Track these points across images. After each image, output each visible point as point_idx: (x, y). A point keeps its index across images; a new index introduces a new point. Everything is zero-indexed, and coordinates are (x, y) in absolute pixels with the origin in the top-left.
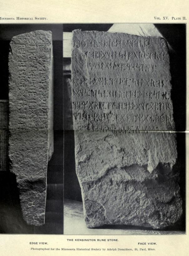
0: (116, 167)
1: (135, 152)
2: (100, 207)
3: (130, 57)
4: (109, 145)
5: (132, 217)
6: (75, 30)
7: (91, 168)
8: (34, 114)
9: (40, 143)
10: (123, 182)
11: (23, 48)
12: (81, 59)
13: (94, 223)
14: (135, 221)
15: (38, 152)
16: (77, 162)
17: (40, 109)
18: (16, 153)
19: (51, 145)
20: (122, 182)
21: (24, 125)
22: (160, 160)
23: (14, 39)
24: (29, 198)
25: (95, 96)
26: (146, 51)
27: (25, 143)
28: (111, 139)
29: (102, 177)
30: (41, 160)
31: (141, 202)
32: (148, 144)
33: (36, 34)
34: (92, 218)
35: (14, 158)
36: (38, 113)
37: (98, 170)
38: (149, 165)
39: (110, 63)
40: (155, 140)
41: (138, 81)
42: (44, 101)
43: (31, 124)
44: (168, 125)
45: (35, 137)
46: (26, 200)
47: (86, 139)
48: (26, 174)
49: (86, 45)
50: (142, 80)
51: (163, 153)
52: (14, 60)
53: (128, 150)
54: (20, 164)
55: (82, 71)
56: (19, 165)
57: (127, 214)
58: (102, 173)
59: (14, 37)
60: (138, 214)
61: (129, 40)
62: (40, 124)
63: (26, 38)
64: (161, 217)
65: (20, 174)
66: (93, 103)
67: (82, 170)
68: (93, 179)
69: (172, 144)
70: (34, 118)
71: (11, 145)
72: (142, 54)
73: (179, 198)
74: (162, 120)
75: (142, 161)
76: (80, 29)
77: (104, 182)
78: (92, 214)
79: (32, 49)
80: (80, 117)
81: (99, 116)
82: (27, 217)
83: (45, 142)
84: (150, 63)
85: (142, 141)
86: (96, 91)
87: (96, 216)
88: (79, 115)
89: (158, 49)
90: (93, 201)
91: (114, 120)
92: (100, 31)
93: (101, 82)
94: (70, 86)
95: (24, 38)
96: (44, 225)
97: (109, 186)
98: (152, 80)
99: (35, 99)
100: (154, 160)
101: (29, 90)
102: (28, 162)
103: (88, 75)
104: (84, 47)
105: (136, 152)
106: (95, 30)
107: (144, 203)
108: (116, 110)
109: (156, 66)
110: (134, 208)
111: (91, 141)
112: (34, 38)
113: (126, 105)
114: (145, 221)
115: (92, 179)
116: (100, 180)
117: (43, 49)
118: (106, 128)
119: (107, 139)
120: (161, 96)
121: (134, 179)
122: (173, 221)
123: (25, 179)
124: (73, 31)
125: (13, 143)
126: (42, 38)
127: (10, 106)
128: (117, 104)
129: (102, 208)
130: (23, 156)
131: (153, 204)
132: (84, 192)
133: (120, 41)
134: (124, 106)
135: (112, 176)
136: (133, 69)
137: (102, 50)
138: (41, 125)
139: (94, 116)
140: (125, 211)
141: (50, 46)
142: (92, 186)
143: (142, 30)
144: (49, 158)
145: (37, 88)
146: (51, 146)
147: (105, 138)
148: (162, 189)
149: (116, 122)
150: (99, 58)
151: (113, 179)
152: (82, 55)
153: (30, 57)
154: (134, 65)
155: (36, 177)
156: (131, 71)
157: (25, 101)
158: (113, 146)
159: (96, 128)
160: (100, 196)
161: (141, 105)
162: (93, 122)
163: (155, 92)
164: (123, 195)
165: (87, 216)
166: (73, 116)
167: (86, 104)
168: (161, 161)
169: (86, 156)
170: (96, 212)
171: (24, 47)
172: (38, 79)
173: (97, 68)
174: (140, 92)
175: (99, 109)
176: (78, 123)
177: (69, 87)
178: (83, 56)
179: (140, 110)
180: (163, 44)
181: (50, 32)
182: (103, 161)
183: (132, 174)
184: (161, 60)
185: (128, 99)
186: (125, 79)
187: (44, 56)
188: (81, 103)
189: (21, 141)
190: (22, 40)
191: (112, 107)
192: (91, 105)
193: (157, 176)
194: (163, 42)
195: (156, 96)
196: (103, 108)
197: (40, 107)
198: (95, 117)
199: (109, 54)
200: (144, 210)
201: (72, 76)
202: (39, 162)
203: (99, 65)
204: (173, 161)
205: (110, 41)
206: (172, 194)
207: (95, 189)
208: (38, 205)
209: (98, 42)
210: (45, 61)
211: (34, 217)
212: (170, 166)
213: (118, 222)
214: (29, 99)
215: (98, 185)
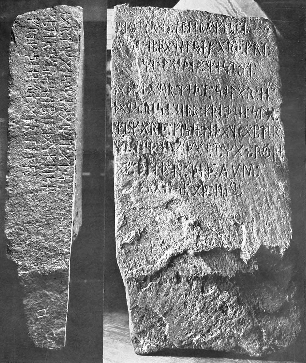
0: (185, 252)
1: (219, 228)
2: (157, 320)
3: (211, 50)
4: (174, 216)
5: (213, 336)
6: (119, 6)
7: (142, 253)
8: (50, 142)
9: (59, 212)
10: (198, 277)
11: (34, 35)
12: (127, 52)
13: (148, 347)
14: (219, 343)
15: (56, 227)
16: (118, 243)
17: (61, 135)
18: (16, 227)
19: (77, 214)
20: (196, 278)
21: (33, 161)
22: (262, 242)
23: (18, 19)
24: (39, 303)
25: (151, 114)
26: (239, 40)
27: (33, 211)
28: (177, 205)
29: (162, 270)
30: (60, 239)
31: (229, 311)
32: (241, 215)
33: (56, 12)
34: (144, 337)
35: (14, 236)
36: (58, 140)
37: (155, 257)
38: (242, 249)
39: (176, 60)
40: (255, 207)
41: (226, 90)
42: (67, 120)
43: (44, 159)
44: (277, 163)
45: (50, 200)
46: (34, 306)
47: (135, 206)
48: (34, 263)
49: (138, 30)
50: (232, 87)
51: (268, 230)
52: (18, 55)
53: (207, 225)
54: (24, 246)
55: (130, 73)
56: (23, 248)
57: (205, 331)
58: (161, 261)
59: (20, 16)
60: (223, 331)
61: (210, 22)
62: (60, 159)
63: (40, 18)
64: (264, 337)
65: (24, 263)
66: (147, 124)
67: (127, 257)
68: (145, 272)
69: (284, 216)
70: (50, 149)
71: (9, 214)
72: (232, 46)
73: (295, 305)
74: (266, 154)
75: (230, 242)
76: (127, 3)
77: (164, 277)
78: (143, 331)
79: (49, 36)
80: (126, 148)
81: (158, 147)
82: (35, 334)
83: (68, 209)
84: (245, 61)
85: (232, 209)
86: (153, 105)
87: (152, 334)
88: (124, 144)
89: (260, 38)
90: (146, 309)
91: (183, 152)
92: (160, 7)
93: (161, 90)
94: (110, 96)
95: (36, 17)
96: (63, 348)
97: (173, 285)
98: (248, 88)
99: (52, 118)
100: (252, 242)
101: (43, 103)
102: (37, 242)
103: (141, 79)
104: (134, 34)
105: (221, 227)
106: (152, 6)
107: (235, 313)
108: (187, 137)
109: (256, 66)
110: (217, 321)
111: (142, 208)
112: (52, 18)
113: (205, 129)
114: (237, 344)
115: (144, 272)
116: (158, 274)
117: (68, 35)
118: (169, 165)
119: (170, 205)
120: (263, 115)
121: (217, 272)
122: (284, 344)
123: (33, 270)
124: (115, 7)
125: (12, 212)
126: (65, 18)
127: (11, 129)
128: (188, 127)
129: (162, 321)
130: (29, 232)
131: (250, 314)
132: (130, 295)
133: (195, 23)
134: (200, 131)
135: (179, 268)
136: (216, 69)
137: (164, 39)
138: (62, 160)
139: (150, 147)
140: (202, 327)
141: (79, 32)
142: (144, 284)
143: (232, 5)
144: (74, 236)
145: (57, 99)
146: (78, 217)
147: (168, 203)
148: (266, 290)
149: (186, 156)
150: (158, 50)
151: (180, 274)
152: (129, 46)
153: (45, 49)
154: (218, 63)
155: (51, 268)
156: (213, 73)
157: (36, 120)
158: (180, 217)
159: (152, 165)
160: (158, 300)
161: (231, 128)
162: (147, 156)
163: (254, 108)
164: (197, 299)
165: (136, 334)
166: (114, 146)
167: (135, 126)
168: (265, 243)
169: (134, 234)
170: (152, 327)
171: (35, 33)
172: (58, 85)
173: (154, 66)
174: (229, 108)
175: (159, 134)
176: (122, 158)
177: (107, 98)
178: (131, 47)
179: (228, 137)
180: (268, 29)
181: (79, 8)
182: (163, 242)
183: (213, 264)
184: (264, 56)
185: (207, 118)
186: (202, 86)
187: (69, 47)
188: (127, 125)
189: (25, 207)
190: (33, 21)
191: (180, 132)
192: (145, 128)
193: (257, 267)
194: (268, 27)
195: (255, 115)
196: (164, 133)
197: (61, 131)
198: (152, 149)
199: (175, 45)
200: (234, 324)
201: (113, 79)
202: (58, 242)
203: (158, 63)
204: (286, 244)
205: (177, 24)
206: (282, 299)
207: (150, 289)
208: (55, 315)
209: (157, 25)
210: (70, 56)
211: (47, 335)
212: (279, 252)
213: (188, 345)
214: (41, 117)
215: (154, 283)
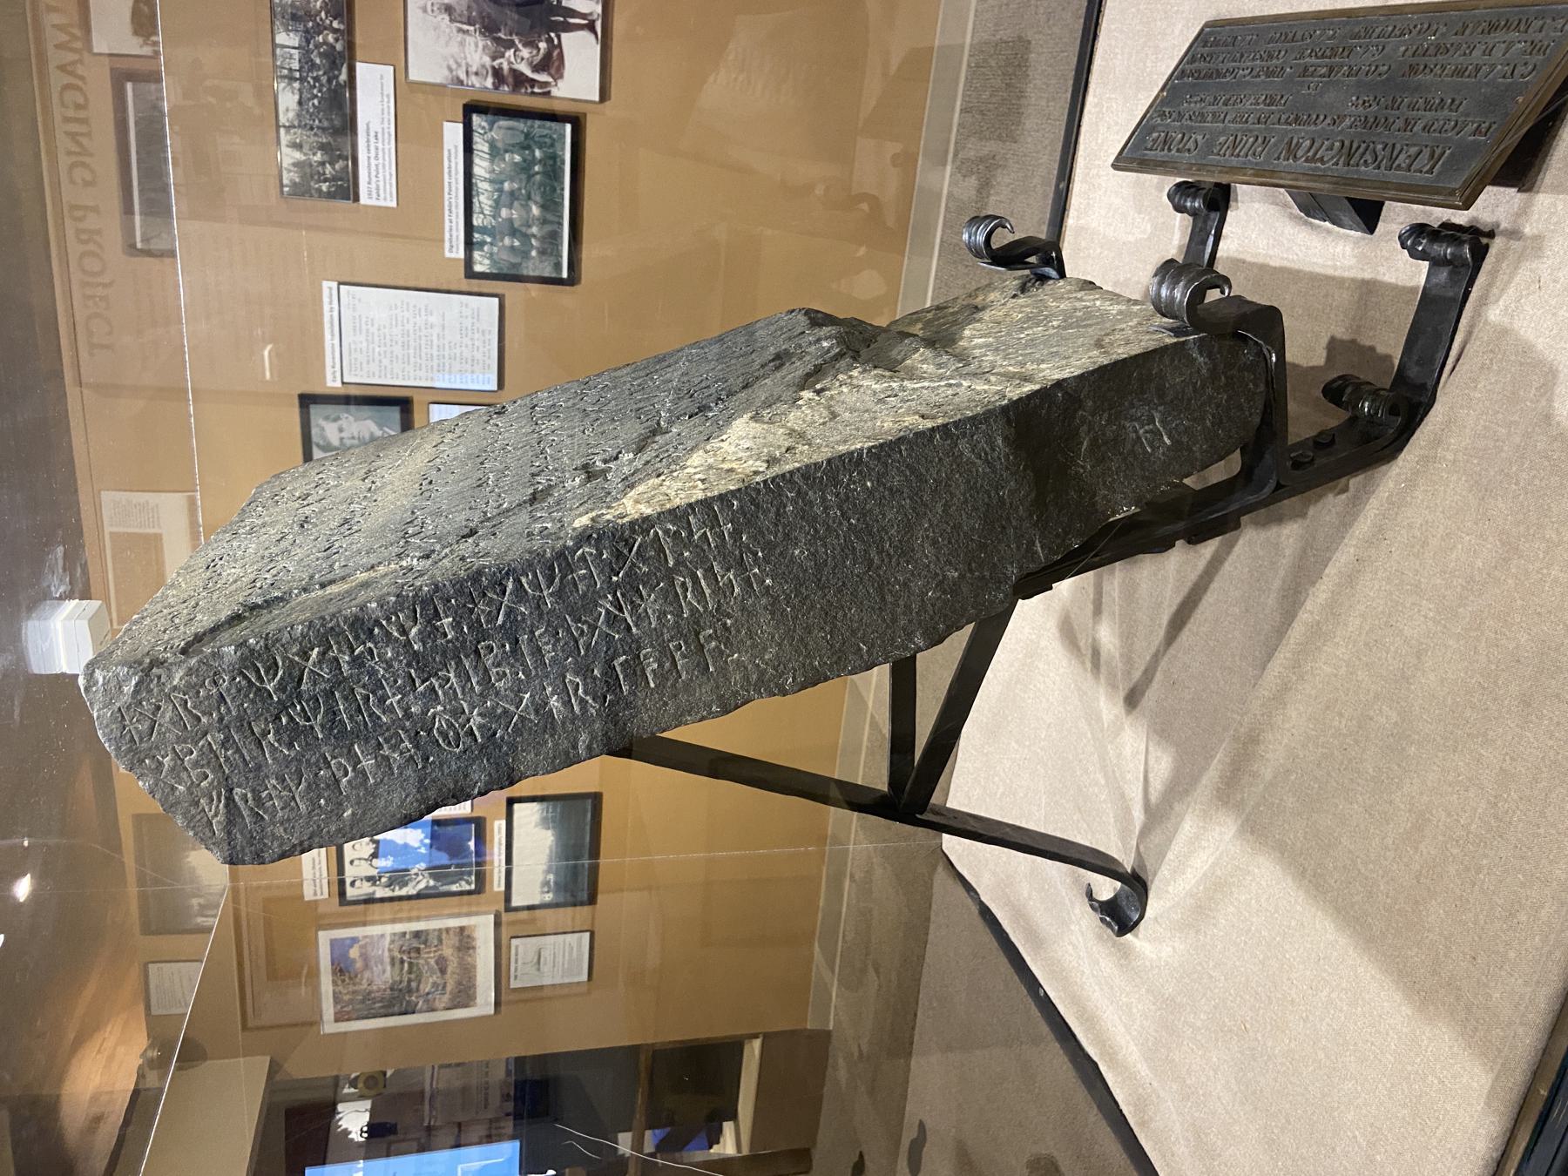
95: (193, 812)
187: (245, 677)
